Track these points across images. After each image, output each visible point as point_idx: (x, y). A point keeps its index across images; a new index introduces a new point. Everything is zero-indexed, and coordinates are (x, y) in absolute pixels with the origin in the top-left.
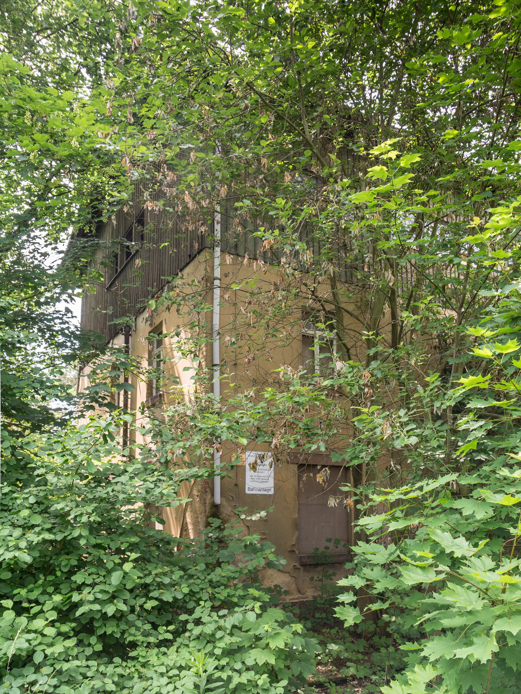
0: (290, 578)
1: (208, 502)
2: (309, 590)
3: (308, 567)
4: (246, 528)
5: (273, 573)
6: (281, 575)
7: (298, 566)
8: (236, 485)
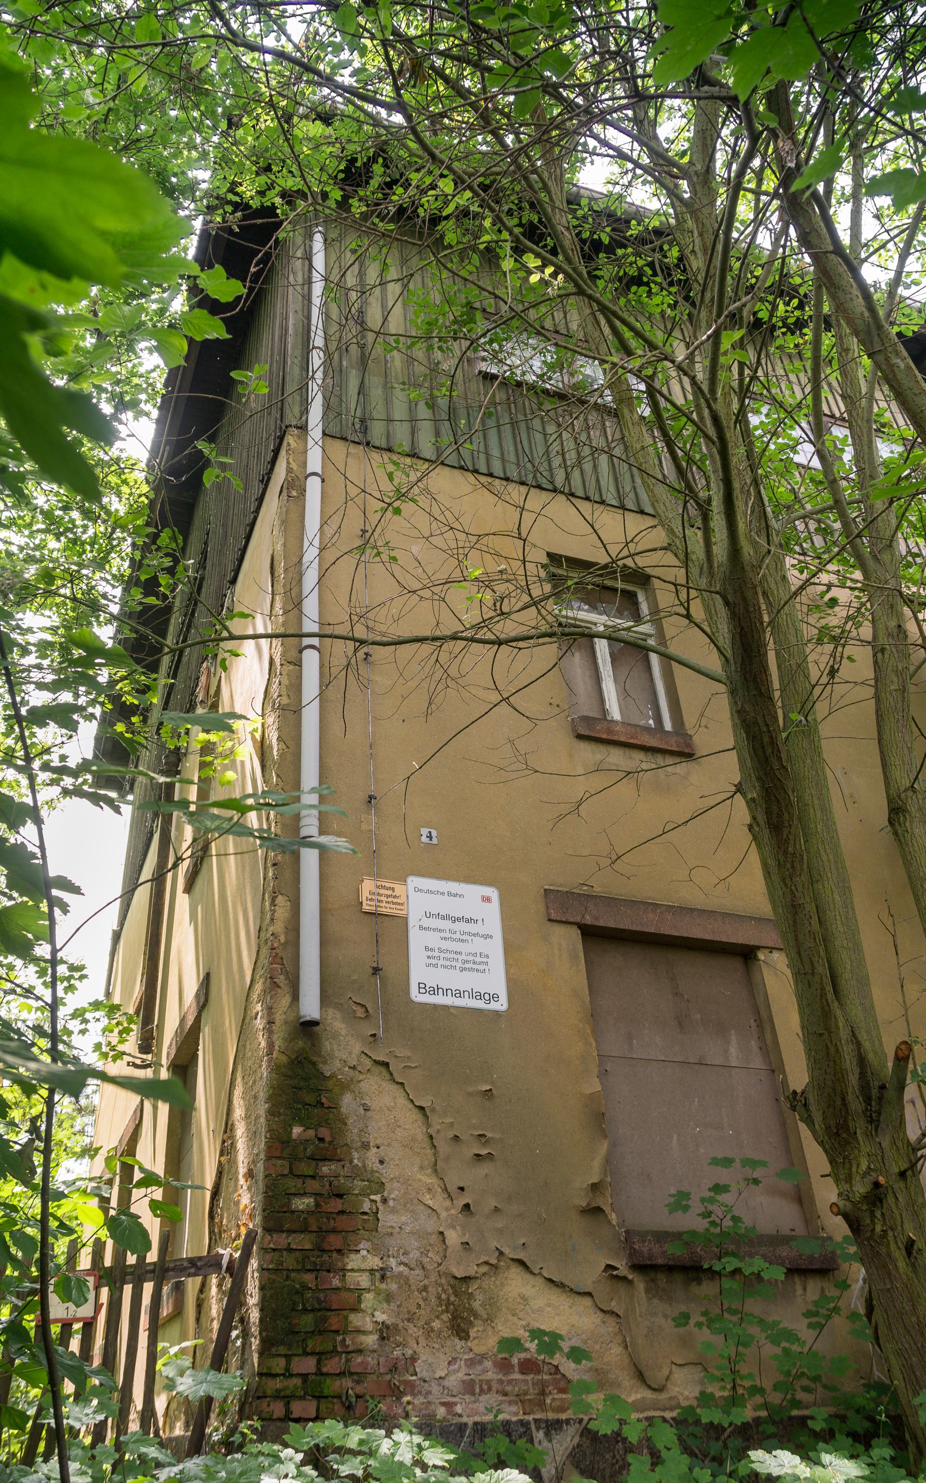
0: (597, 1318)
1: (279, 1018)
2: (679, 1375)
3: (662, 1279)
4: (416, 1115)
5: (528, 1291)
6: (562, 1301)
7: (623, 1268)
8: (376, 970)
